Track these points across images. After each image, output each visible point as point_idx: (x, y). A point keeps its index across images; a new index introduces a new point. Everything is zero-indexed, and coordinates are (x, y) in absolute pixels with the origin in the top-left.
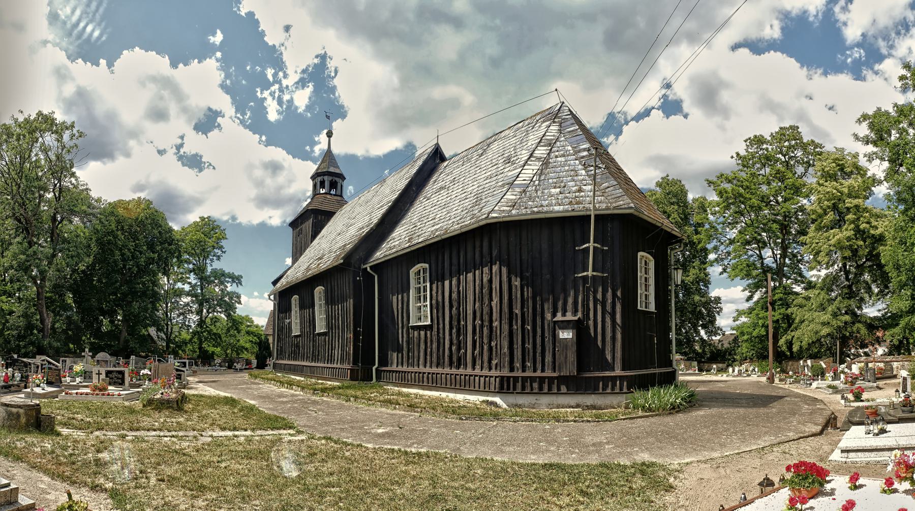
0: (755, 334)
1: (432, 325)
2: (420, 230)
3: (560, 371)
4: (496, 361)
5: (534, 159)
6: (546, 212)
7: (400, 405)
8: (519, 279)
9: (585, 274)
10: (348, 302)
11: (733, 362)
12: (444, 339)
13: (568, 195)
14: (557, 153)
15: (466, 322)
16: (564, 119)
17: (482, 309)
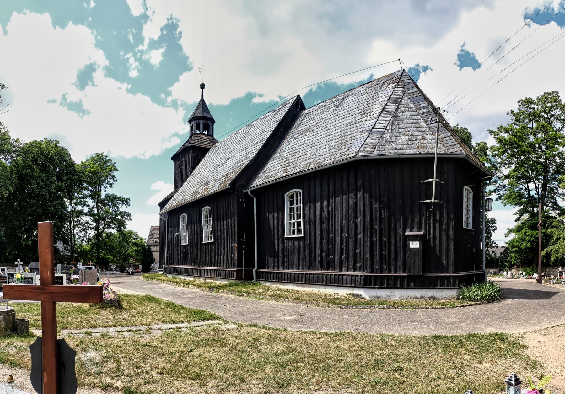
0: (523, 246)
1: (305, 236)
2: (294, 163)
3: (410, 272)
4: (360, 264)
5: (386, 112)
6: (400, 154)
7: (287, 298)
8: (378, 203)
9: (429, 201)
10: (232, 219)
11: (504, 267)
12: (315, 247)
13: (415, 141)
14: (403, 109)
15: (335, 235)
16: (406, 83)
17: (349, 225)
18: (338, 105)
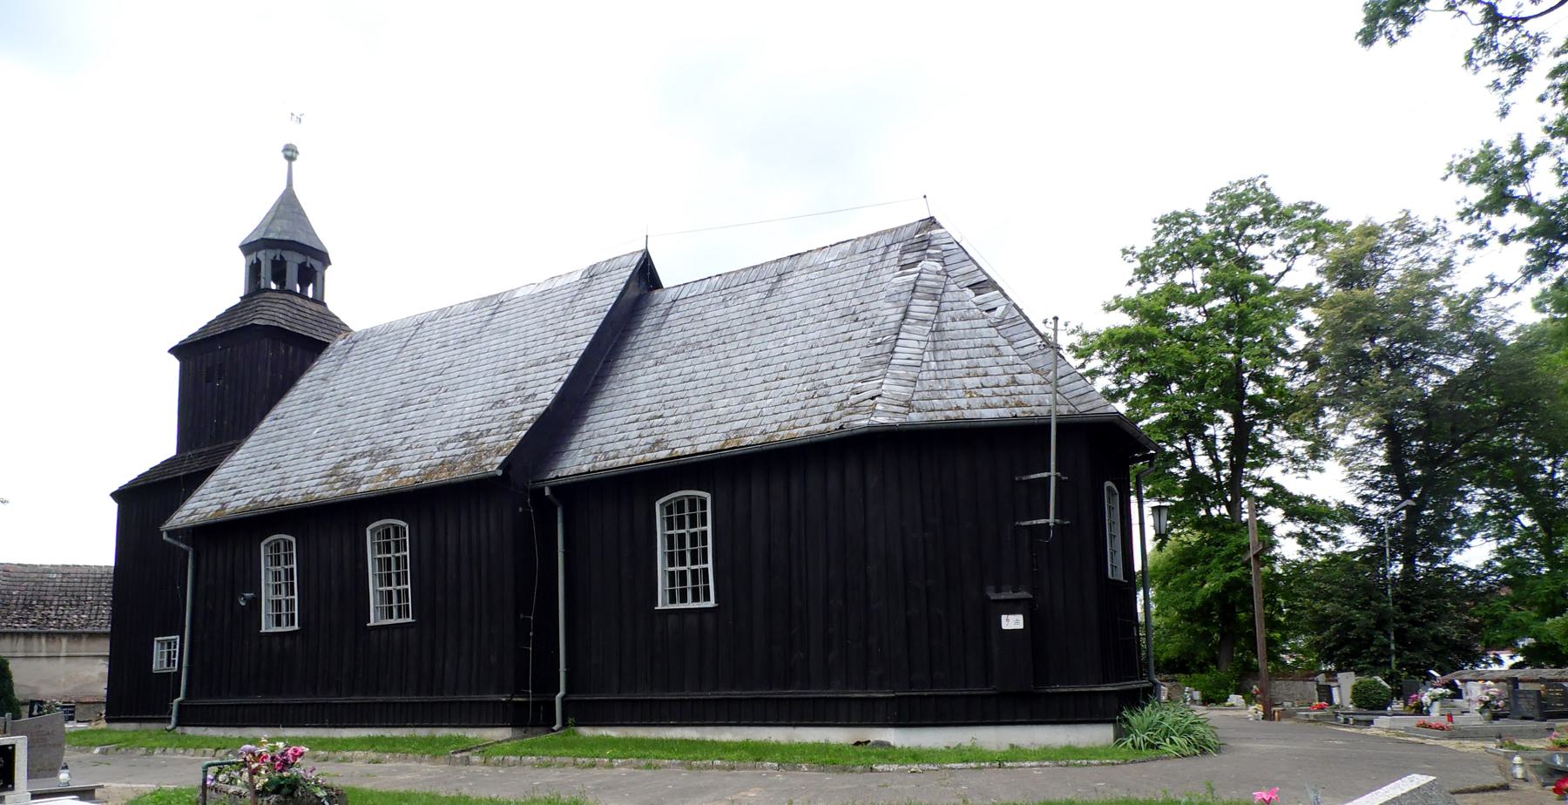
18: (771, 290)
